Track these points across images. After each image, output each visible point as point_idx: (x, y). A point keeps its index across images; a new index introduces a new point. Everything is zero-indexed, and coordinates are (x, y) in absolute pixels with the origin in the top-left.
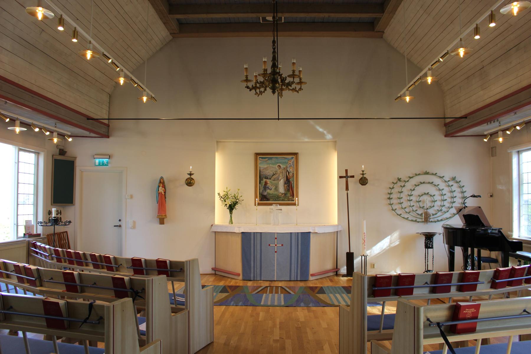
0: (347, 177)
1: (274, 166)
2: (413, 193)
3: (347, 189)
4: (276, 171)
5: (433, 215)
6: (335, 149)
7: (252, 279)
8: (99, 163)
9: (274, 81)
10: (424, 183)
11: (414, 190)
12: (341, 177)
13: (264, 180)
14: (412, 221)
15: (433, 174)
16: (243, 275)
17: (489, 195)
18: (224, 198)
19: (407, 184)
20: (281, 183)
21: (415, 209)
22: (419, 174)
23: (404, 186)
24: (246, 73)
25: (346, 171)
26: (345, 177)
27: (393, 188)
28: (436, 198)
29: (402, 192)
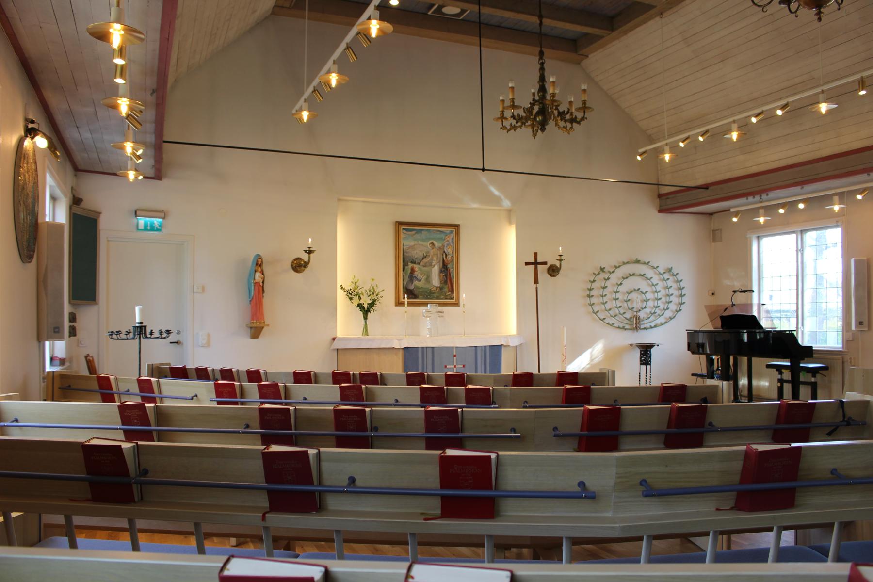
0: (536, 263)
1: (425, 244)
2: (620, 288)
3: (536, 282)
4: (428, 252)
6: (510, 223)
8: (146, 225)
9: (541, 114)
10: (634, 274)
11: (621, 284)
13: (410, 265)
14: (619, 328)
15: (644, 263)
17: (711, 292)
18: (351, 294)
19: (612, 276)
20: (436, 270)
22: (628, 263)
23: (608, 279)
24: (513, 94)
25: (536, 254)
27: (594, 281)
28: (649, 296)
29: (605, 287)
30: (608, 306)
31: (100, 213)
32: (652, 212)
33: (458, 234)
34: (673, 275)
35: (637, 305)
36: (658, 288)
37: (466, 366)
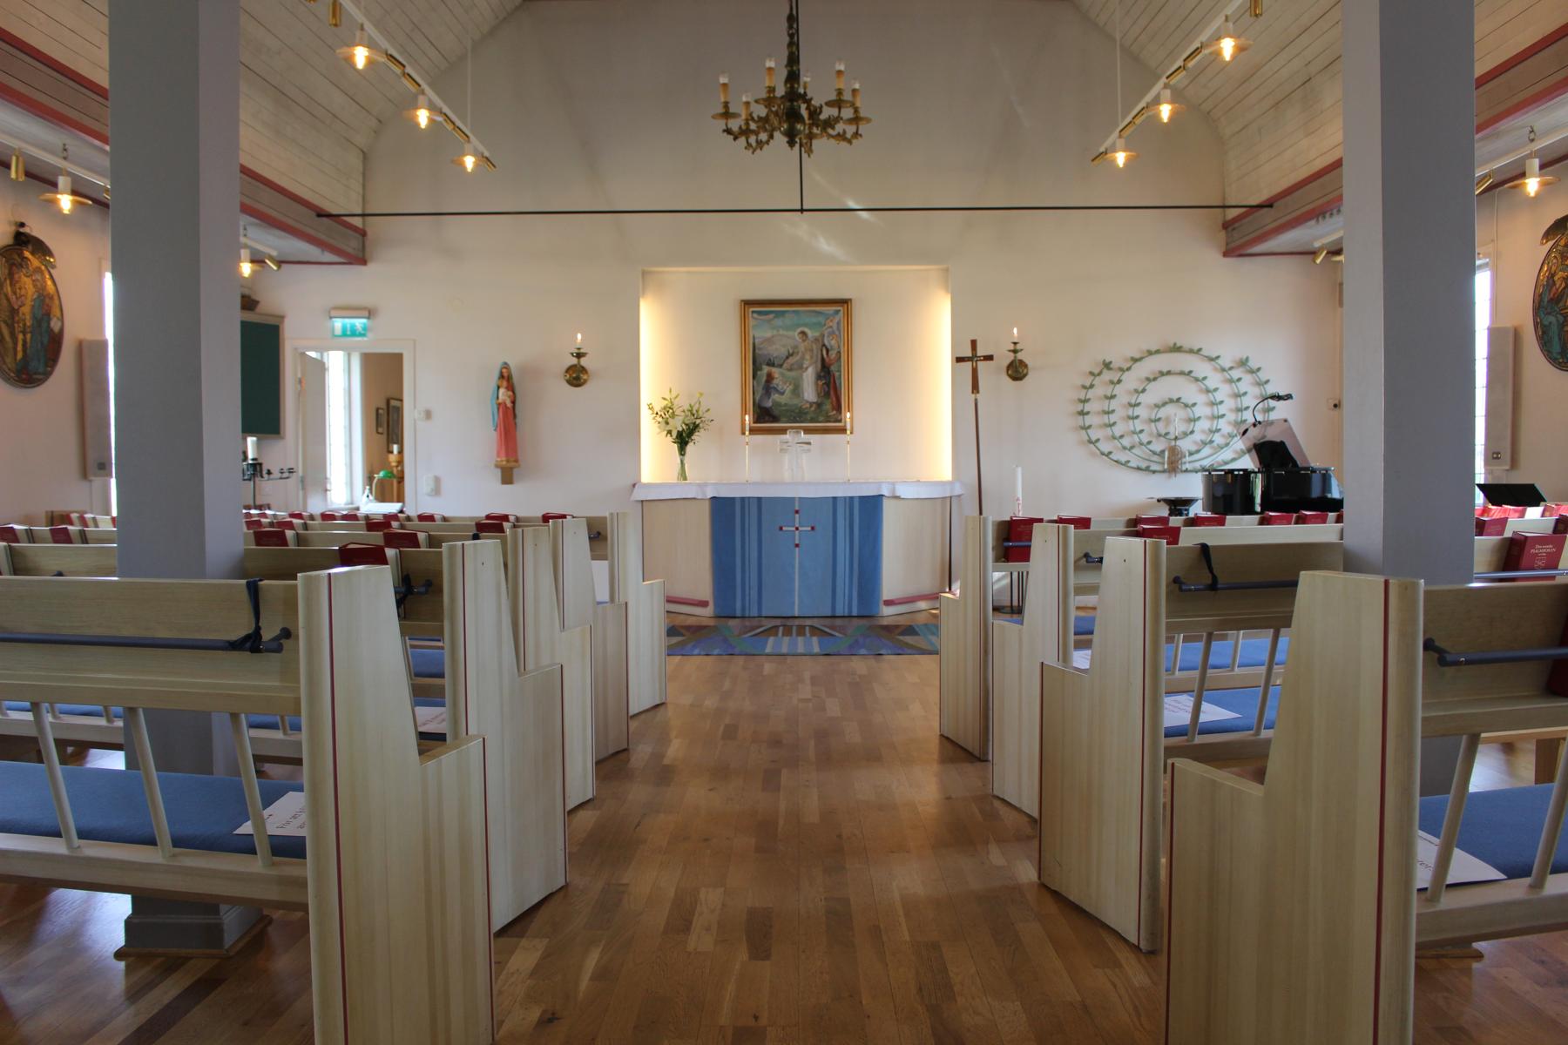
2: (1142, 398)
3: (975, 388)
5: (1191, 454)
6: (947, 289)
7: (738, 613)
8: (344, 329)
10: (1169, 373)
11: (1144, 391)
12: (959, 360)
13: (766, 369)
14: (1139, 469)
15: (1191, 351)
16: (716, 605)
20: (809, 377)
21: (1144, 438)
22: (1158, 352)
23: (1119, 381)
25: (974, 343)
26: (970, 359)
27: (1092, 386)
29: (1113, 397)
30: (1118, 430)
31: (282, 317)
32: (1212, 257)
33: (848, 315)
34: (1252, 372)
35: (1178, 427)
36: (1219, 396)
37: (818, 528)
